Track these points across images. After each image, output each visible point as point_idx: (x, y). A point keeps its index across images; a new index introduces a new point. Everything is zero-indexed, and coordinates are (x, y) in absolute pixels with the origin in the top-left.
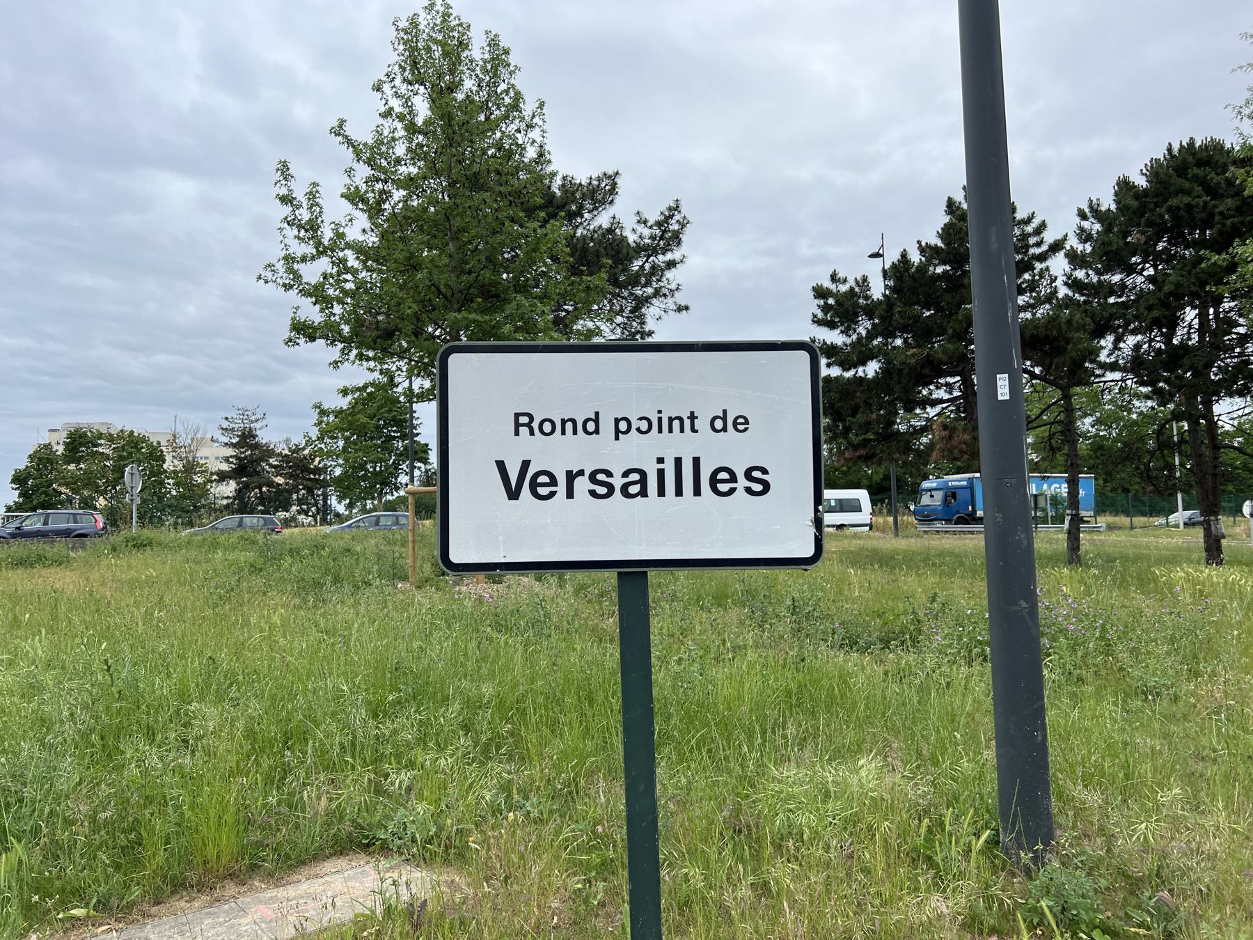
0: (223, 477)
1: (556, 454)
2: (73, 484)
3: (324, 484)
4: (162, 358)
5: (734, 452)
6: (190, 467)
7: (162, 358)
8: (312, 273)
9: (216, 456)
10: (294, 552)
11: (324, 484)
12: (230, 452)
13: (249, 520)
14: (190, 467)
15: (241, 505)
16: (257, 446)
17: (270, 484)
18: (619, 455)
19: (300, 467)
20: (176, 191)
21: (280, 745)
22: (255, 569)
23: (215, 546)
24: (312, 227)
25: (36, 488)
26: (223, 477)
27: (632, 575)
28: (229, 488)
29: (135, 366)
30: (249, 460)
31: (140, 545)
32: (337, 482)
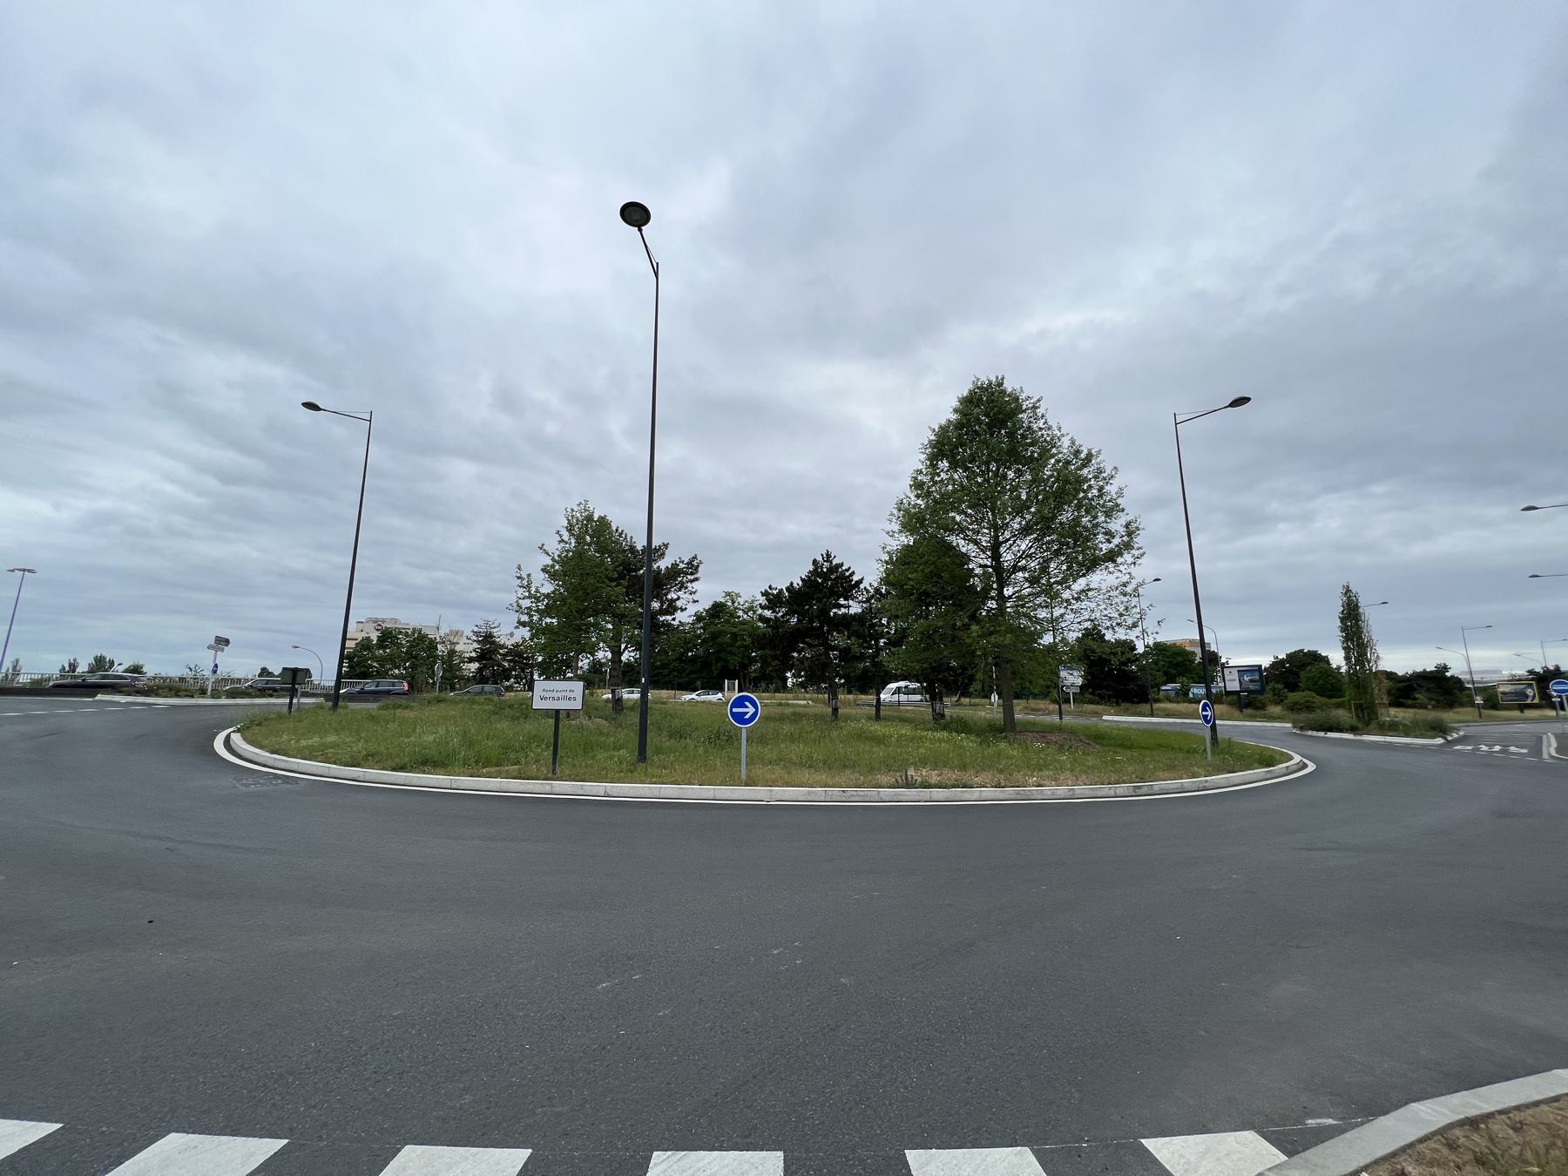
0: (471, 660)
1: (547, 695)
2: (381, 660)
3: (532, 666)
4: (439, 574)
5: (570, 695)
6: (452, 653)
7: (439, 574)
8: (526, 603)
9: (467, 648)
10: (511, 707)
11: (532, 666)
12: (476, 645)
13: (488, 687)
14: (452, 653)
15: (480, 678)
16: (494, 643)
17: (499, 665)
18: (556, 695)
19: (518, 656)
20: (463, 471)
21: (506, 748)
22: (495, 713)
23: (474, 702)
24: (528, 587)
25: (358, 664)
26: (471, 660)
27: (557, 711)
28: (474, 666)
29: (420, 578)
30: (488, 647)
31: (439, 701)
32: (540, 665)
